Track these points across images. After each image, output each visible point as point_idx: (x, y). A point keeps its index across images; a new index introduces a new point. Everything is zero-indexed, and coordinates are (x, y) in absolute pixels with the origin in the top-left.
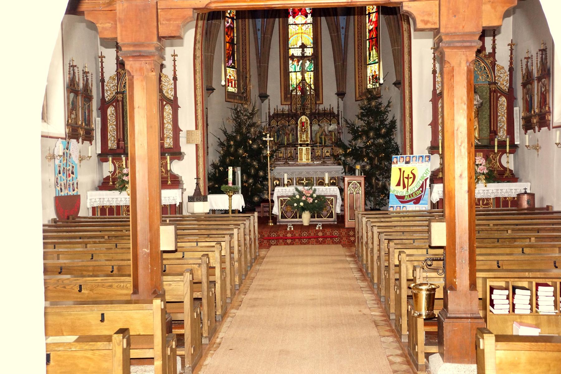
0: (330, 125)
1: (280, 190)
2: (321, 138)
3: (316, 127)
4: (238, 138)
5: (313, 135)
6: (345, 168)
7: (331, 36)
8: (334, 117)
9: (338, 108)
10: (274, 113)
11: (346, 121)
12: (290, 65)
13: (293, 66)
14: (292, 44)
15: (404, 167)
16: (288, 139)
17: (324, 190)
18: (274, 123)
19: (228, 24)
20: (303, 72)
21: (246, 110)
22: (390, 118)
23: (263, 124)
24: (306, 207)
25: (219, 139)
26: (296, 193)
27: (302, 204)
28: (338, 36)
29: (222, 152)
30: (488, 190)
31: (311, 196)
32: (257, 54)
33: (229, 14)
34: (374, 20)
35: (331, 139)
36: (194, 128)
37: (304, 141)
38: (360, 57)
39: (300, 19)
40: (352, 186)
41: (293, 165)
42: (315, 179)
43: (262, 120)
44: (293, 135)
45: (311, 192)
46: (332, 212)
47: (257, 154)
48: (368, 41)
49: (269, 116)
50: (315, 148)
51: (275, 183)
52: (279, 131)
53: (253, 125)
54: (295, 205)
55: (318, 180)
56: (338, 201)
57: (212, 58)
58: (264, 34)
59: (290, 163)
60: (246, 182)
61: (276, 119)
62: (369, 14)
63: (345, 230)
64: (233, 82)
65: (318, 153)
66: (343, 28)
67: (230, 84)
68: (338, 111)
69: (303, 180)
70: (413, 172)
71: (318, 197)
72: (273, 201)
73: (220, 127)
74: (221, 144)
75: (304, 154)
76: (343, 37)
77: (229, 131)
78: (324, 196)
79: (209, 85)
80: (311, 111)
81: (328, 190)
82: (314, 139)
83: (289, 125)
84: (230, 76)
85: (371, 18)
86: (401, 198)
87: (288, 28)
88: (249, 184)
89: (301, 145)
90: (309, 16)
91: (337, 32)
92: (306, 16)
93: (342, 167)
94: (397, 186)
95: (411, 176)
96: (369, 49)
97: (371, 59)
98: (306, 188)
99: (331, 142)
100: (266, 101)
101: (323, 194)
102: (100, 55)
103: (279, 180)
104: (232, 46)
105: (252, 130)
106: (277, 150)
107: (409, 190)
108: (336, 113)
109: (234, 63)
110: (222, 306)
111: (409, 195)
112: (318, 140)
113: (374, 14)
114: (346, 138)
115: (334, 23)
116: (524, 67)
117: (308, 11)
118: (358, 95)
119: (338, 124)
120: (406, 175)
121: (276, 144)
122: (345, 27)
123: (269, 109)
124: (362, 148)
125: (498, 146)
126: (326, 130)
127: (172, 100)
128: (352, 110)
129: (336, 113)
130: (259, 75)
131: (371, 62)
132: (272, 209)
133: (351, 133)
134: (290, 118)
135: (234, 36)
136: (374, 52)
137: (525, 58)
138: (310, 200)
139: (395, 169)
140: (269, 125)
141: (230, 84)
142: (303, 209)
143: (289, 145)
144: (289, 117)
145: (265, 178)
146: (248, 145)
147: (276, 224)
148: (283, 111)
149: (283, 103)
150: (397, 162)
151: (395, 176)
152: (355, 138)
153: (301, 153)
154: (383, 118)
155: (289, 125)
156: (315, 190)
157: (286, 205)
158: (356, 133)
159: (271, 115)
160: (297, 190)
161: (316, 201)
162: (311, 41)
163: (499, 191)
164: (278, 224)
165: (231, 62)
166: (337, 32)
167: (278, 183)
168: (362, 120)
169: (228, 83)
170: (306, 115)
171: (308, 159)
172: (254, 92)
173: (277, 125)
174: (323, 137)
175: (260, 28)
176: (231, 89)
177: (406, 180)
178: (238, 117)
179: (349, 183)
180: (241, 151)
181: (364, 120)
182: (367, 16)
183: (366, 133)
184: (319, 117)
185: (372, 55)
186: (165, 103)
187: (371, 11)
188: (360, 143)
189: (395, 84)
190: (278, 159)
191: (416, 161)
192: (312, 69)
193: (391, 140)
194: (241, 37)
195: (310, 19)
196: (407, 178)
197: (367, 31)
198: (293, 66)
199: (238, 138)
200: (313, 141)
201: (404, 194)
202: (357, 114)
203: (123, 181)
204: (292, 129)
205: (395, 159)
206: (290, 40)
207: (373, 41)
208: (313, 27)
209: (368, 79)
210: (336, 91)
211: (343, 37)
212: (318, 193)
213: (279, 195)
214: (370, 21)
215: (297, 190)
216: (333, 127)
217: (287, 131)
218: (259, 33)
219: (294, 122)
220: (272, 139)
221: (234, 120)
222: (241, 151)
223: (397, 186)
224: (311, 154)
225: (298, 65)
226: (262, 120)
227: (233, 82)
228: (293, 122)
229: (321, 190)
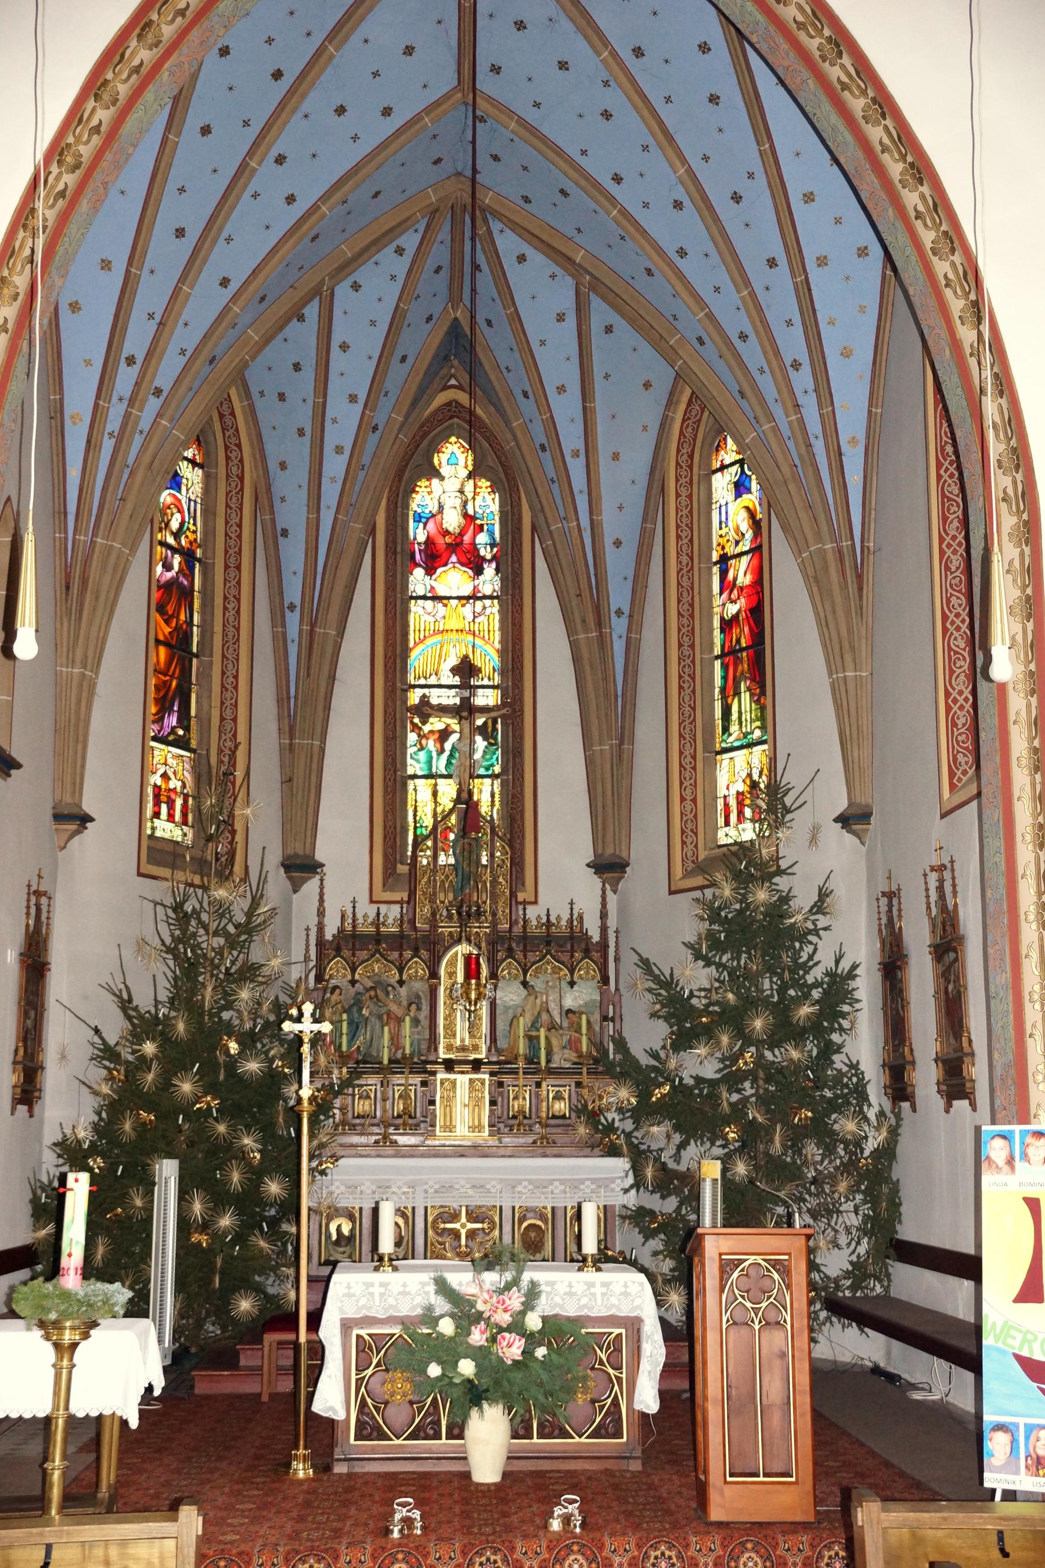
0: (572, 984)
1: (358, 1289)
2: (532, 1040)
3: (510, 994)
4: (181, 1027)
5: (501, 1025)
6: (637, 1169)
7: (574, 646)
8: (587, 953)
9: (604, 915)
10: (341, 930)
11: (646, 965)
12: (410, 751)
13: (422, 756)
14: (420, 671)
16: (396, 1041)
17: (579, 1289)
18: (337, 971)
19: (169, 575)
20: (467, 773)
21: (222, 910)
22: (825, 959)
23: (296, 973)
24: (485, 1382)
25: (97, 1031)
26: (441, 1305)
27: (467, 1367)
28: (603, 643)
29: (105, 1089)
31: (517, 1326)
32: (283, 699)
33: (177, 535)
34: (744, 579)
35: (573, 1044)
37: (463, 1049)
38: (687, 720)
39: (453, 579)
40: (745, 1283)
41: (411, 1152)
42: (507, 1214)
43: (287, 957)
44: (416, 1022)
45: (515, 1300)
46: (616, 1403)
47: (258, 1101)
48: (718, 664)
49: (321, 943)
50: (507, 1079)
51: (333, 1228)
52: (358, 1004)
53: (249, 973)
54: (434, 1370)
55: (522, 1219)
56: (647, 1348)
57: (87, 690)
58: (313, 626)
59: (402, 1140)
60: (205, 1227)
61: (346, 953)
63: (714, 1542)
64: (179, 802)
65: (521, 1100)
66: (619, 613)
67: (164, 808)
68: (604, 929)
69: (455, 1217)
71: (555, 1329)
72: (318, 1351)
73: (106, 979)
74: (108, 1053)
75: (462, 1105)
76: (619, 647)
77: (143, 1001)
78: (578, 1321)
79: (68, 799)
80: (494, 924)
81: (598, 1290)
82: (502, 1043)
83: (401, 983)
84: (165, 776)
85: (730, 576)
87: (406, 611)
88: (217, 1237)
89: (449, 1065)
90: (489, 571)
91: (599, 624)
93: (621, 1165)
94: (1019, 1299)
96: (723, 690)
97: (734, 728)
98: (491, 1278)
99: (573, 1056)
100: (311, 886)
101: (571, 1312)
103: (351, 1217)
104: (181, 659)
105: (245, 994)
106: (346, 1083)
108: (596, 938)
109: (187, 729)
112: (522, 1048)
113: (745, 560)
114: (645, 1034)
115: (586, 593)
116: (934, 896)
117: (486, 553)
118: (678, 872)
119: (605, 980)
121: (343, 1059)
122: (626, 610)
123: (321, 913)
124: (713, 1083)
126: (553, 1007)
128: (665, 928)
129: (596, 938)
130: (288, 781)
131: (732, 740)
132: (314, 1381)
133: (666, 1019)
134: (408, 954)
135: (190, 623)
136: (744, 704)
137: (932, 869)
138: (512, 1349)
140: (319, 978)
141: (164, 808)
142: (475, 1395)
143: (399, 1064)
144: (401, 949)
145: (291, 1207)
146: (222, 1059)
147: (328, 1468)
148: (376, 923)
149: (380, 894)
150: (1010, 1162)
152: (682, 1041)
153: (449, 1102)
154: (797, 954)
155: (401, 983)
156: (532, 1294)
157: (385, 1366)
158: (687, 1024)
159: (328, 936)
160: (443, 1288)
161: (541, 1352)
164: (340, 1469)
165: (174, 720)
166: (599, 624)
167: (346, 1230)
168: (708, 963)
169: (157, 803)
171: (477, 1128)
172: (260, 820)
173: (353, 982)
174: (542, 1033)
175: (297, 602)
176: (166, 829)
178: (184, 938)
179: (726, 1267)
180: (186, 1087)
181: (719, 966)
182: (716, 570)
183: (733, 1019)
184: (525, 951)
185: (735, 716)
187: (730, 550)
188: (700, 1063)
189: (844, 820)
190: (350, 1125)
192: (497, 769)
193: (828, 1050)
194: (218, 627)
195: (490, 581)
197: (716, 623)
198: (422, 756)
199: (181, 1027)
200: (499, 1052)
202: (692, 938)
204: (415, 1001)
205: (999, 1143)
206: (414, 654)
207: (737, 661)
209: (720, 803)
210: (590, 857)
211: (619, 647)
212: (545, 1306)
213: (351, 1313)
215: (443, 1288)
216: (581, 995)
217: (393, 1007)
218: (293, 621)
219: (422, 971)
220: (326, 1027)
221: (169, 950)
222: (186, 1087)
223: (1019, 1299)
224: (493, 1103)
225: (441, 751)
226: (287, 957)
227: (179, 802)
228: (417, 968)
229: (569, 1291)
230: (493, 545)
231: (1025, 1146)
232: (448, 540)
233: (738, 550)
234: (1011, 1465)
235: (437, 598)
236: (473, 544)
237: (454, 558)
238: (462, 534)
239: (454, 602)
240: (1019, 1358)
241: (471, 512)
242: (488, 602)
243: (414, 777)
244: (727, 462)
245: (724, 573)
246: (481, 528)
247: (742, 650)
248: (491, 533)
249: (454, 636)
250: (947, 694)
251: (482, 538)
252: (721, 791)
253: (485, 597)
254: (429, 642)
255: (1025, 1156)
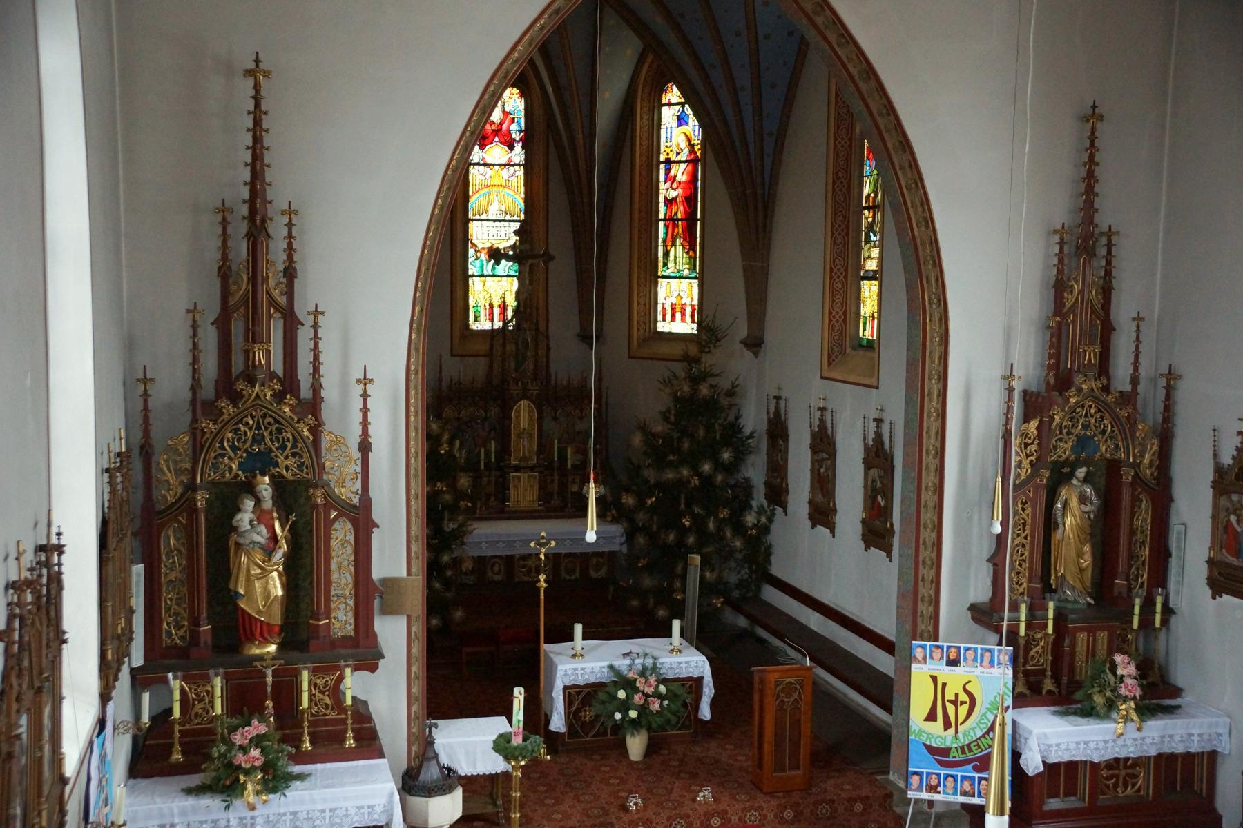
12: (470, 260)
13: (478, 263)
15: (946, 673)
27: (633, 714)
30: (1143, 739)
36: (404, 574)
62: (668, 162)
67: (678, 315)
70: (968, 687)
85: (672, 173)
86: (939, 753)
89: (517, 469)
92: (511, 148)
94: (945, 730)
95: (963, 697)
96: (665, 241)
97: (671, 264)
102: (141, 376)
107: (960, 735)
110: (131, 639)
111: (962, 748)
113: (683, 166)
117: (516, 136)
120: (950, 695)
125: (1132, 614)
127: (355, 507)
139: (920, 675)
141: (678, 315)
150: (925, 659)
151: (920, 698)
162: (521, 204)
163: (1167, 739)
170: (527, 398)
177: (951, 709)
186: (333, 514)
187: (673, 157)
191: (975, 659)
195: (518, 154)
196: (955, 702)
201: (948, 744)
203: (230, 765)
205: (919, 650)
206: (472, 200)
208: (526, 174)
214: (670, 179)
230: (520, 131)
231: (931, 652)
232: (493, 127)
233: (678, 158)
234: (919, 789)
235: (485, 165)
236: (509, 131)
237: (496, 139)
238: (501, 124)
239: (497, 167)
240: (925, 745)
241: (507, 110)
242: (517, 168)
243: (473, 276)
244: (672, 101)
245: (668, 171)
246: (513, 120)
247: (678, 220)
248: (519, 124)
249: (496, 189)
250: (830, 313)
251: (514, 127)
252: (661, 300)
253: (515, 165)
254: (482, 192)
255: (931, 657)
